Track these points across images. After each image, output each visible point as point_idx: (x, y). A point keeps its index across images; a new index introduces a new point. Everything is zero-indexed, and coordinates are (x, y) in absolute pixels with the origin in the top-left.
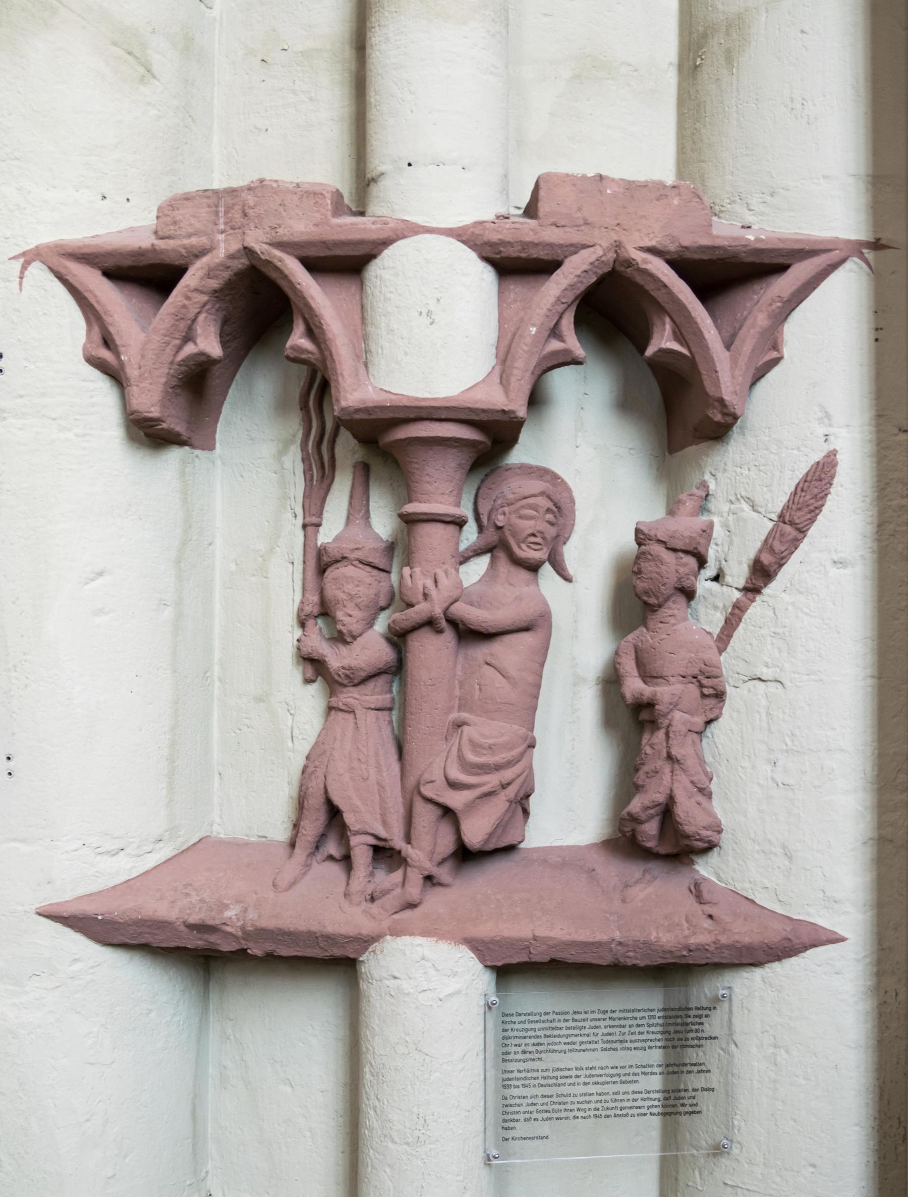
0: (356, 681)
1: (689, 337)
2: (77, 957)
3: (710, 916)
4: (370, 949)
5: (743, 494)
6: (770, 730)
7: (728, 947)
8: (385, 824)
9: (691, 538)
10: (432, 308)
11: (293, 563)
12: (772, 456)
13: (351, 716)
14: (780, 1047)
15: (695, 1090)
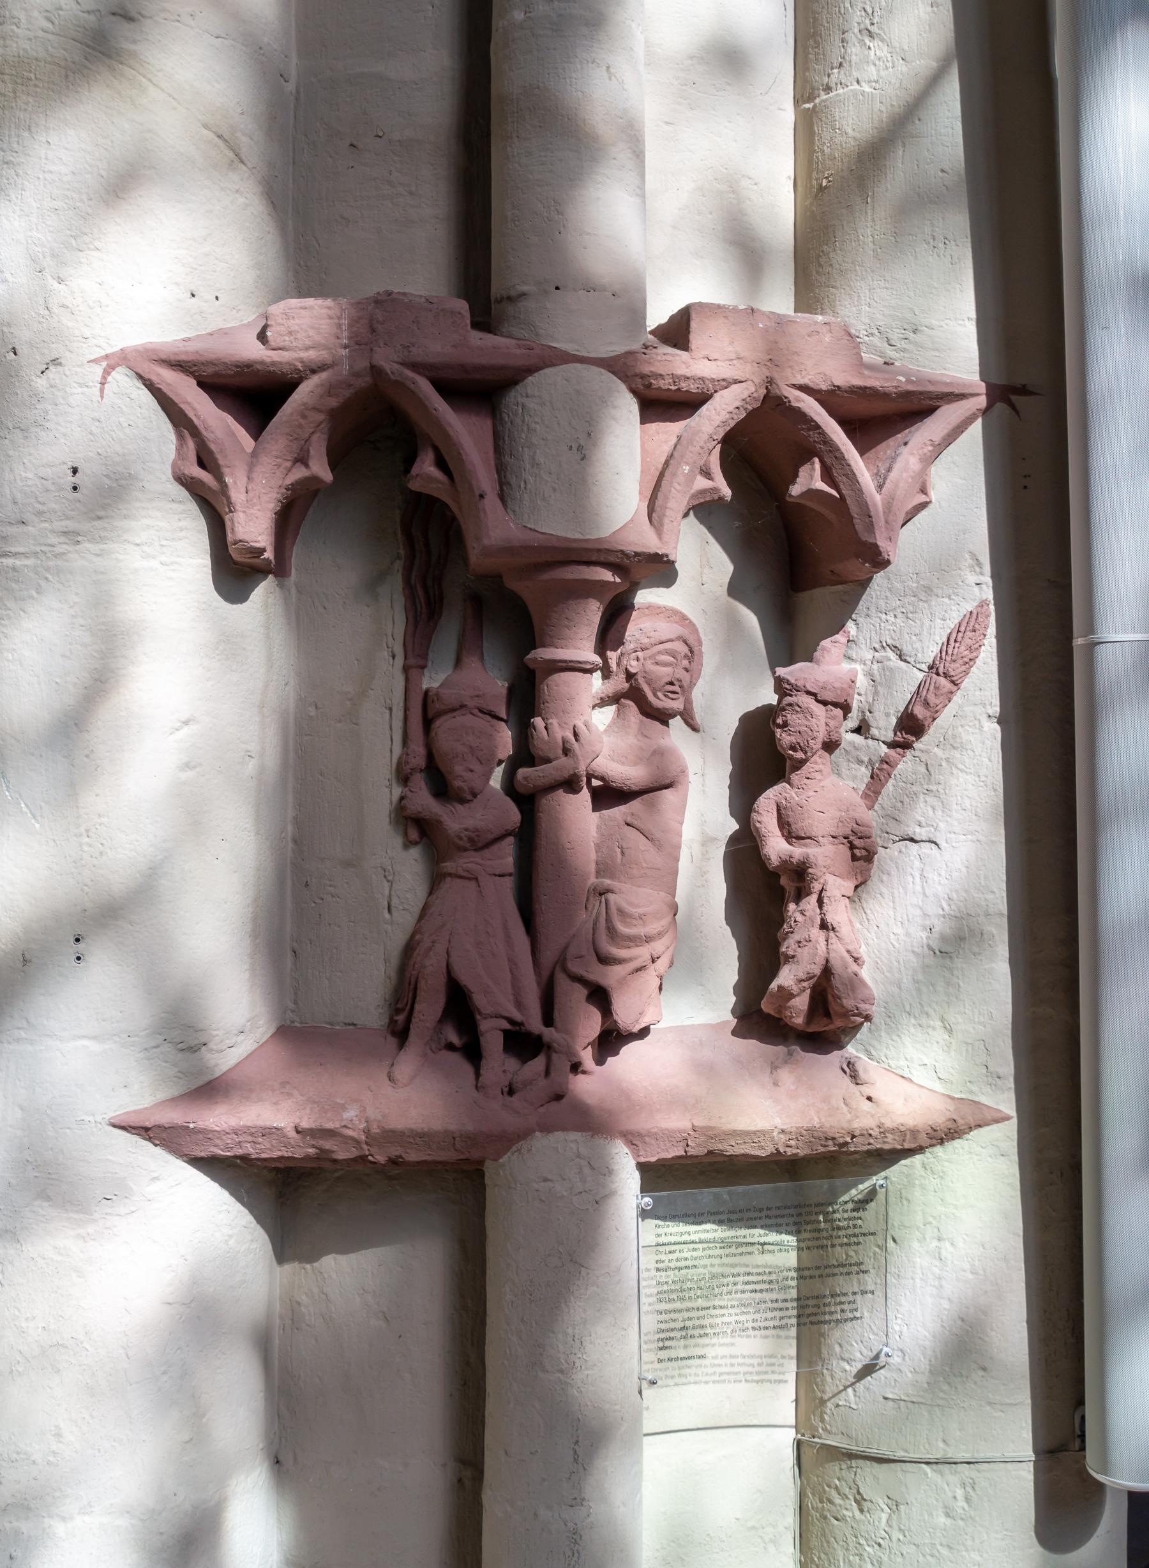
0: (480, 845)
1: (840, 479)
2: (155, 1175)
3: (869, 1099)
4: (514, 1148)
5: (889, 642)
6: (925, 895)
7: (893, 1131)
8: (519, 1005)
9: (842, 689)
10: (582, 443)
11: (391, 709)
12: (921, 603)
13: (473, 884)
14: (944, 1240)
15: (854, 1293)
